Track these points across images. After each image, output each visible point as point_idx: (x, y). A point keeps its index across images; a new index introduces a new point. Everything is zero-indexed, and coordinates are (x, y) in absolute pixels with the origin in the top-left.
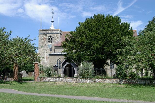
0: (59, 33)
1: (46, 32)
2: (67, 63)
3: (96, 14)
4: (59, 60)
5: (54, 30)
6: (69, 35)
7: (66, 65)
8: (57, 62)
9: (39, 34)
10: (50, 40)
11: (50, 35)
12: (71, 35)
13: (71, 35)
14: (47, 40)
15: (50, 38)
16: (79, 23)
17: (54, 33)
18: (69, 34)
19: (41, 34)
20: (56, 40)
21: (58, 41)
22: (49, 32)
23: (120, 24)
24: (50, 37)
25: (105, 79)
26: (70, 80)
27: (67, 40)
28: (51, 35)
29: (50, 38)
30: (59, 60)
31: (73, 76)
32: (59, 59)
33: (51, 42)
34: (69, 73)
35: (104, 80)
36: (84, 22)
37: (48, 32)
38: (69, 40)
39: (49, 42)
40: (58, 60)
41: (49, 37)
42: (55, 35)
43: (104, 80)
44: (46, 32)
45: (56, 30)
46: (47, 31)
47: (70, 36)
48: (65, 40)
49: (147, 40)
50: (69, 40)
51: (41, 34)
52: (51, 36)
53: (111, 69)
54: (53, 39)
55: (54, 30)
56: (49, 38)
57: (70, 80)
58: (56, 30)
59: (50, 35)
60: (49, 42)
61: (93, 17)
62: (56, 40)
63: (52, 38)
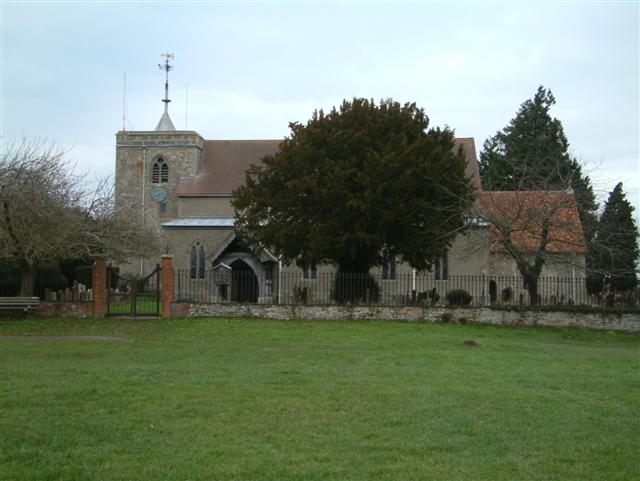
3: (350, 100)
4: (198, 248)
6: (260, 168)
12: (265, 167)
13: (265, 165)
14: (146, 173)
15: (160, 165)
16: (292, 125)
17: (176, 144)
18: (259, 164)
20: (181, 172)
23: (426, 131)
25: (380, 309)
26: (273, 311)
27: (250, 183)
29: (160, 165)
31: (256, 301)
33: (165, 180)
34: (243, 288)
35: (378, 312)
37: (151, 143)
38: (257, 182)
43: (378, 312)
44: (146, 143)
47: (264, 169)
48: (245, 185)
50: (257, 182)
53: (437, 277)
54: (171, 166)
57: (273, 311)
61: (338, 110)
63: (165, 165)
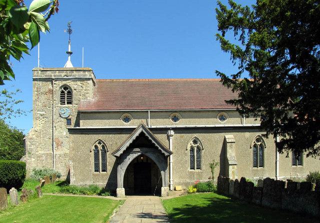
0: (89, 79)
1: (55, 76)
2: (135, 152)
4: (100, 147)
5: (76, 70)
7: (131, 160)
8: (93, 152)
9: (34, 80)
10: (67, 95)
11: (64, 82)
14: (57, 97)
15: (66, 92)
17: (77, 77)
19: (40, 80)
20: (81, 97)
21: (88, 98)
22: (63, 74)
24: (66, 87)
28: (68, 83)
29: (66, 92)
30: (100, 147)
32: (100, 143)
33: (69, 103)
36: (217, 10)
39: (63, 103)
40: (96, 147)
41: (61, 88)
42: (79, 83)
44: (55, 76)
45: (81, 70)
46: (57, 73)
49: (47, 17)
51: (40, 80)
52: (68, 84)
54: (74, 92)
55: (76, 70)
56: (62, 92)
58: (81, 70)
59: (64, 82)
60: (63, 103)
62: (81, 97)
